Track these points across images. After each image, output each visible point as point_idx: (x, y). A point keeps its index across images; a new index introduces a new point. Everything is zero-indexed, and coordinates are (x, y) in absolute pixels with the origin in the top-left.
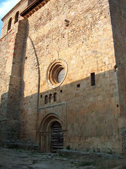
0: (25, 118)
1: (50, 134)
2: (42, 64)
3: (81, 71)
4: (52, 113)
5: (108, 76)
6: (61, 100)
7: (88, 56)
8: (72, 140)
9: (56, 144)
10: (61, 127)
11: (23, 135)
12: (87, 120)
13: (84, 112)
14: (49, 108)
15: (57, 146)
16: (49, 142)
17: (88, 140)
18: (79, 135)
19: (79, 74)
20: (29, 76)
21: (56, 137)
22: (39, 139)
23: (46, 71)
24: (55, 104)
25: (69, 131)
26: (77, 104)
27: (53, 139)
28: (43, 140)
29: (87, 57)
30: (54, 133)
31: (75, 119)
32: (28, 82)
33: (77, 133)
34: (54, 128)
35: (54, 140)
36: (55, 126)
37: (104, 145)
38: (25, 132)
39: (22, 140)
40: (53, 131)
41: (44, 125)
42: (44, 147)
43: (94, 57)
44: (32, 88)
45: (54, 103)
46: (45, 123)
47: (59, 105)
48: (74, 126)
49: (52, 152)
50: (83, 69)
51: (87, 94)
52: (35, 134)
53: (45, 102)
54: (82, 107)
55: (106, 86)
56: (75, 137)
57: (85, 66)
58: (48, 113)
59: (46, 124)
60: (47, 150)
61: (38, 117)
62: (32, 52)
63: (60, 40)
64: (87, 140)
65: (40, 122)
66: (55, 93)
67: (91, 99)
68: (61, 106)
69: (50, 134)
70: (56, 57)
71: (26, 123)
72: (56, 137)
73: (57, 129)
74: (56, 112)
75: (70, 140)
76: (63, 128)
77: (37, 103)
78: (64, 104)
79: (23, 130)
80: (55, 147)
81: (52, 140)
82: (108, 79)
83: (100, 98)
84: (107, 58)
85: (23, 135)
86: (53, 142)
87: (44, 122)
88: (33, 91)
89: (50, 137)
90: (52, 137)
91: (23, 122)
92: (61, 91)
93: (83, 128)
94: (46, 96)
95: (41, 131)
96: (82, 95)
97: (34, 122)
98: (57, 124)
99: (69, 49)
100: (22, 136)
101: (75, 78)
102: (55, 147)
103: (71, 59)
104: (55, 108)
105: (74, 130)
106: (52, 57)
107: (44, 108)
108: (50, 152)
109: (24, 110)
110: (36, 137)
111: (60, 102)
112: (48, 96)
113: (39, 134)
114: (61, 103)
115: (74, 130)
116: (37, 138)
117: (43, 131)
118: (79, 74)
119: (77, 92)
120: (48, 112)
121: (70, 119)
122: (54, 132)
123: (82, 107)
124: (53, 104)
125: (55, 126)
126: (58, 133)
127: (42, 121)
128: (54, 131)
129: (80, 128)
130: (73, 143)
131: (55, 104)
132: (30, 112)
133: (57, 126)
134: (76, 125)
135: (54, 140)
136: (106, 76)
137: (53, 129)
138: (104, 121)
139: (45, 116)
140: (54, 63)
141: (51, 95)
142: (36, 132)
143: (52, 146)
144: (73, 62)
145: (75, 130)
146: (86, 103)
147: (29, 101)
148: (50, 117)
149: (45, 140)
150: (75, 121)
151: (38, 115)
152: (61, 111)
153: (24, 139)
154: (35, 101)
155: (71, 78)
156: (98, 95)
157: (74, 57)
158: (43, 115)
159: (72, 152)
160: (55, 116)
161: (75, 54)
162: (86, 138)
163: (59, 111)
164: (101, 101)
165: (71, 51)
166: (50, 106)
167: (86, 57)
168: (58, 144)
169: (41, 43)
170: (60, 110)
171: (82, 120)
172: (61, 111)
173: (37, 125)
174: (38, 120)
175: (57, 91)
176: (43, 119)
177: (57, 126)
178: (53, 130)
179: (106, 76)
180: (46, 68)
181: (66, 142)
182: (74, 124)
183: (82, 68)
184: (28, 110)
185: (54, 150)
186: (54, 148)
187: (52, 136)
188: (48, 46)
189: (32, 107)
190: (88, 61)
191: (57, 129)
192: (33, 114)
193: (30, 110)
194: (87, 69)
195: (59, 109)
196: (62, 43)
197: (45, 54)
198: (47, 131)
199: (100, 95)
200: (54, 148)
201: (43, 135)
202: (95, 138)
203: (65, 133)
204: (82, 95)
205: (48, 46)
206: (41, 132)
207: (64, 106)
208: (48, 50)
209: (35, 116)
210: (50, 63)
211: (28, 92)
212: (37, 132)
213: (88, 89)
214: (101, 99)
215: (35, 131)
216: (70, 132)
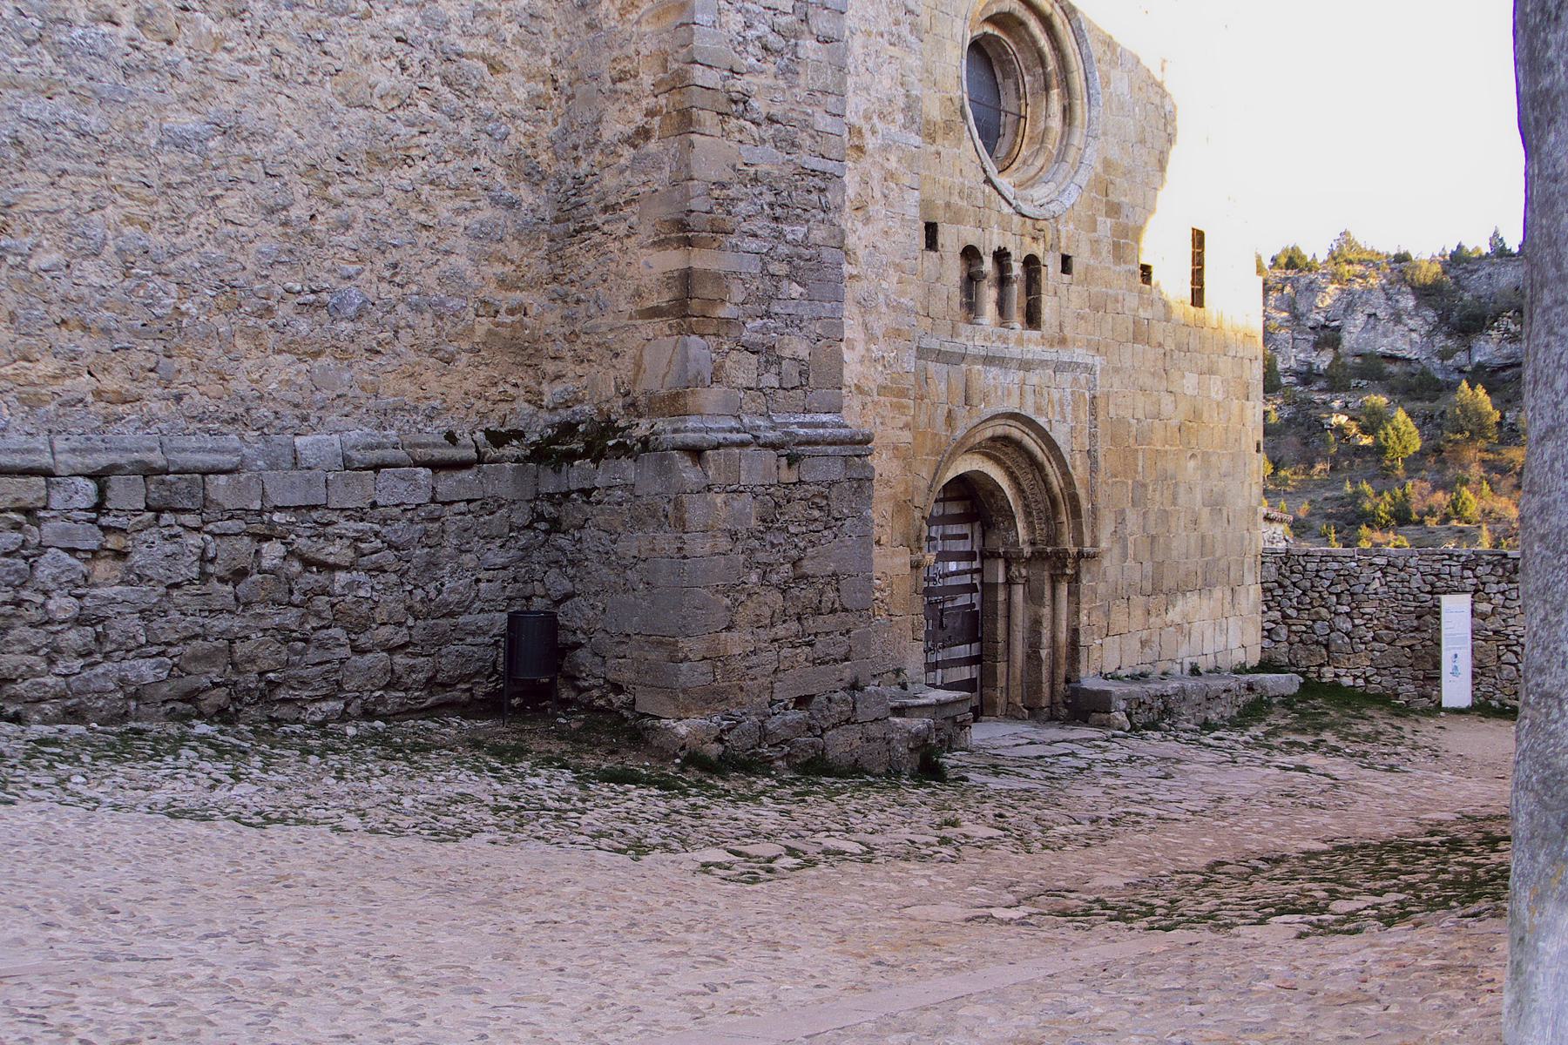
105: (1125, 556)
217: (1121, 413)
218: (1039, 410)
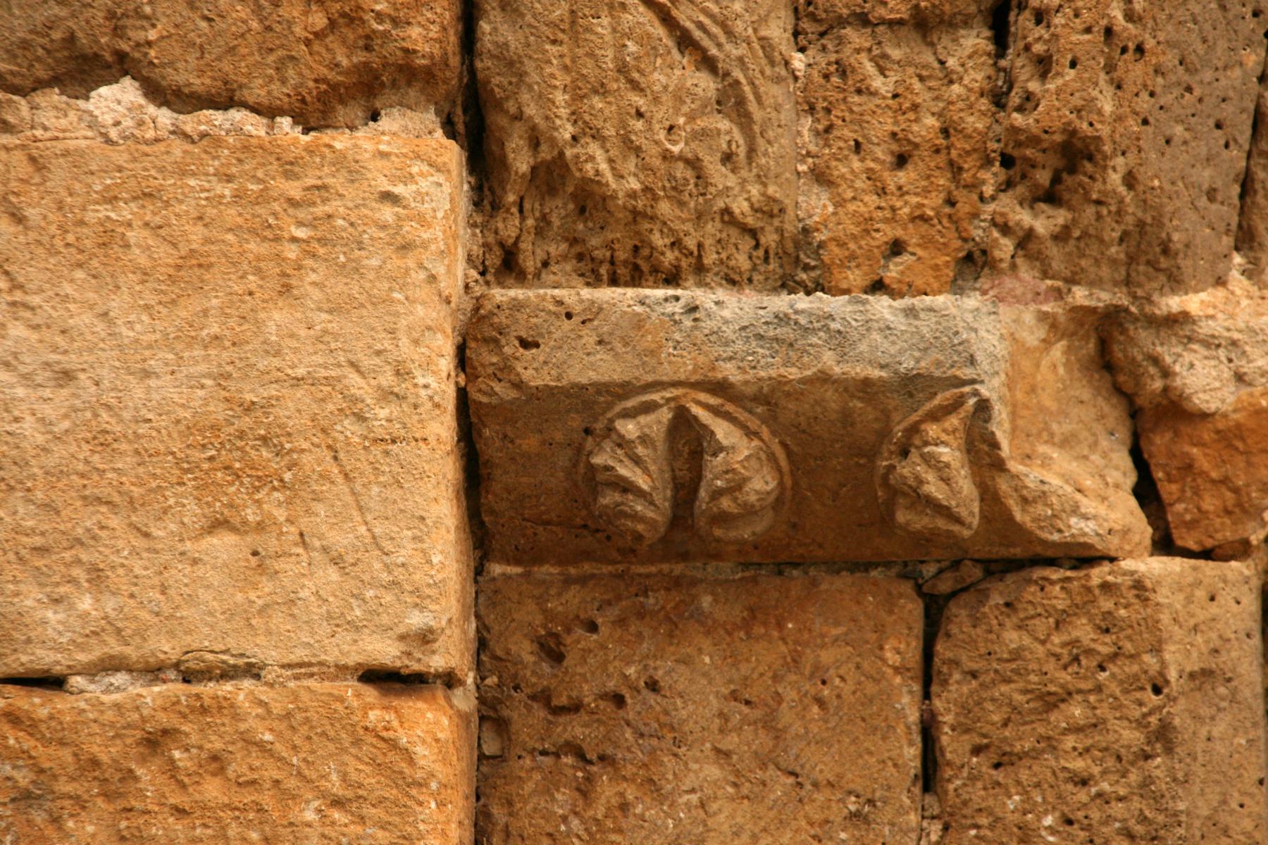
142: (402, 557)
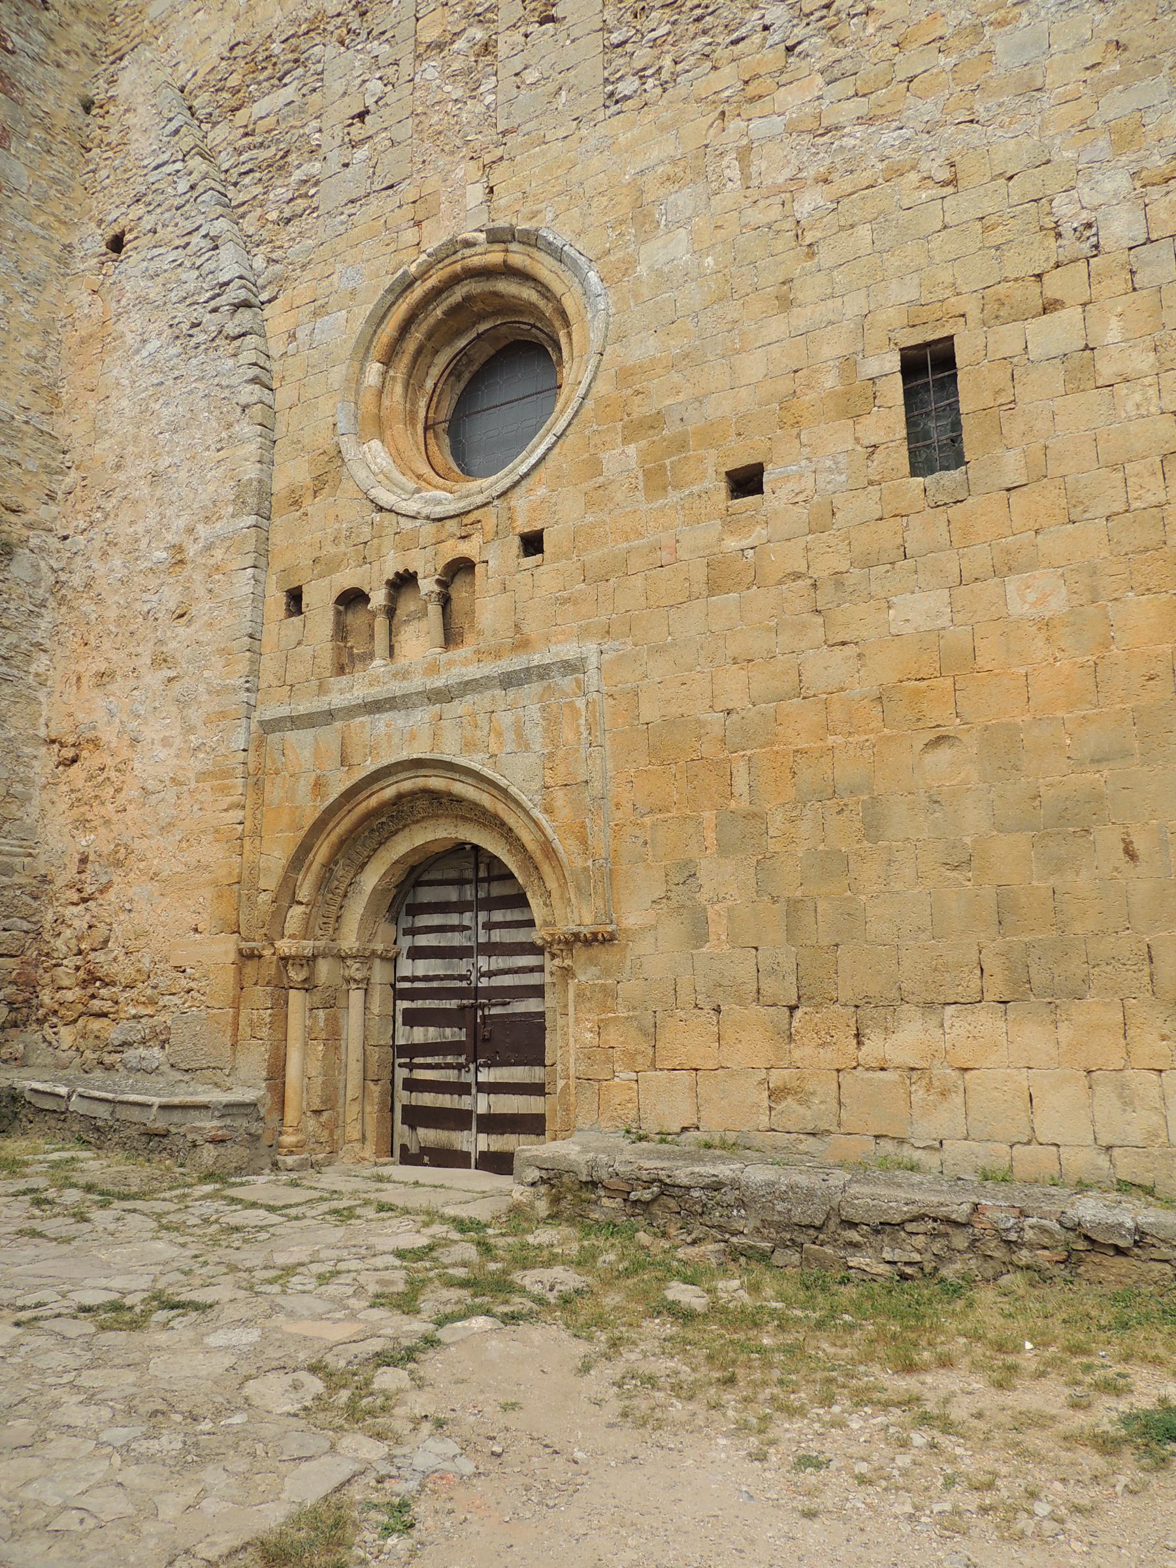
0: (107, 822)
1: (380, 973)
2: (302, 289)
3: (776, 327)
4: (418, 764)
5: (1143, 361)
6: (532, 628)
7: (865, 178)
8: (688, 1040)
9: (451, 1076)
10: (526, 904)
11: (84, 984)
12: (872, 828)
13: (830, 740)
14: (386, 716)
15: (462, 1089)
16: (375, 1055)
17: (906, 1040)
18: (769, 986)
19: (753, 366)
20: (145, 414)
21: (452, 1004)
22: (264, 1032)
23: (346, 351)
24: (462, 665)
25: (642, 947)
26: (735, 661)
27: (413, 1018)
28: (310, 1036)
29: (843, 184)
30: (422, 967)
31: (708, 815)
32: (146, 466)
33: (743, 970)
34: (417, 909)
35: (419, 1035)
36: (427, 895)
37: (1127, 1103)
38: (100, 957)
39: (67, 1035)
40: (406, 942)
41: (324, 882)
42: (317, 1112)
43: (945, 184)
44: (181, 522)
45: (451, 663)
46: (329, 866)
47: (508, 681)
48: (703, 897)
49: (404, 1148)
50: (801, 318)
51: (867, 562)
52: (227, 977)
53: (338, 651)
54: (800, 692)
55: (1114, 467)
56: (718, 1010)
57: (821, 278)
58: (371, 766)
59: (339, 871)
60: (354, 1132)
61: (259, 805)
62: (183, 186)
63: (502, 50)
64: (874, 1047)
65: (275, 856)
66: (460, 568)
67: (918, 609)
68: (536, 687)
69: (380, 973)
70: (462, 215)
71: (119, 864)
72: (452, 1004)
73: (453, 919)
74: (468, 745)
75: (652, 1034)
76: (556, 912)
77: (243, 667)
78: (570, 667)
79: (79, 939)
80: (427, 1099)
81: (401, 1030)
82: (1131, 398)
83: (1031, 596)
84: (1117, 182)
85: (84, 984)
86: (411, 1050)
87: (322, 852)
88: (192, 550)
89: (376, 1009)
90: (403, 1004)
91: (84, 860)
92: (532, 543)
93: (822, 906)
94: (352, 599)
95: (285, 946)
96: (797, 576)
97: (212, 853)
98: (452, 874)
99: (622, 129)
100: (69, 996)
101: (699, 400)
102: (427, 1099)
103: (642, 218)
104: (459, 708)
105: (699, 934)
106: (418, 224)
107: (330, 716)
108: (378, 1153)
109: (95, 743)
110: (236, 1005)
111: (522, 645)
112: (427, 585)
113: (271, 973)
114: (537, 659)
115: (699, 934)
116: (244, 1013)
117: (308, 947)
118: (753, 366)
119: (732, 543)
120: (373, 750)
121: (647, 820)
122: (416, 953)
123: (800, 692)
124: (433, 669)
125: (427, 895)
126: (462, 966)
127: (304, 850)
128: (423, 940)
129: (781, 906)
130: (696, 1070)
131: (462, 665)
132: (162, 753)
133: (451, 894)
134: (723, 882)
135: (419, 1035)
136: (1106, 370)
137: (406, 922)
138: (1108, 838)
139: (334, 792)
140: (430, 283)
141: (404, 582)
142: (233, 956)
143: (403, 1097)
144: (670, 249)
145: (718, 928)
146: (850, 650)
147: (146, 652)
148: (400, 797)
149: (334, 1035)
150: (711, 836)
151: (256, 781)
152: (536, 736)
153: (96, 1025)
154: (221, 651)
155: (646, 411)
156: (1003, 569)
157: (684, 199)
158: (319, 785)
159: (717, 1186)
160: (436, 782)
161: (695, 166)
162: (867, 1015)
163: (510, 736)
164: (1046, 624)
165: (642, 144)
166: (397, 688)
167: (834, 189)
168: (467, 1078)
169: (288, 93)
170: (520, 736)
171: (805, 828)
172: (536, 736)
173: (242, 884)
174: (257, 833)
175: (477, 540)
176: (320, 826)
177: (451, 894)
178: (413, 932)
179: (1106, 370)
180: (343, 327)
181: (609, 1060)
182: (705, 866)
183: (786, 303)
184: (136, 740)
185: (421, 1131)
186: (416, 1117)
187: (400, 995)
188: (362, 116)
189: (182, 703)
190: (864, 231)
191: (463, 928)
192: (202, 776)
193: (166, 742)
194: (855, 305)
195: (505, 719)
196: (531, 76)
197: (330, 196)
198: (350, 941)
199: (1032, 565)
200: (416, 1117)
201: (308, 986)
202: (986, 1021)
203: (592, 961)
204: (797, 576)
205: (362, 116)
206: (285, 959)
207: (566, 683)
208: (362, 153)
209: (224, 790)
210: (388, 281)
211: (144, 565)
212: (248, 956)
213: (869, 504)
214: (1057, 604)
215: (225, 949)
216: (653, 949)
217: (673, 710)
218: (468, 745)
